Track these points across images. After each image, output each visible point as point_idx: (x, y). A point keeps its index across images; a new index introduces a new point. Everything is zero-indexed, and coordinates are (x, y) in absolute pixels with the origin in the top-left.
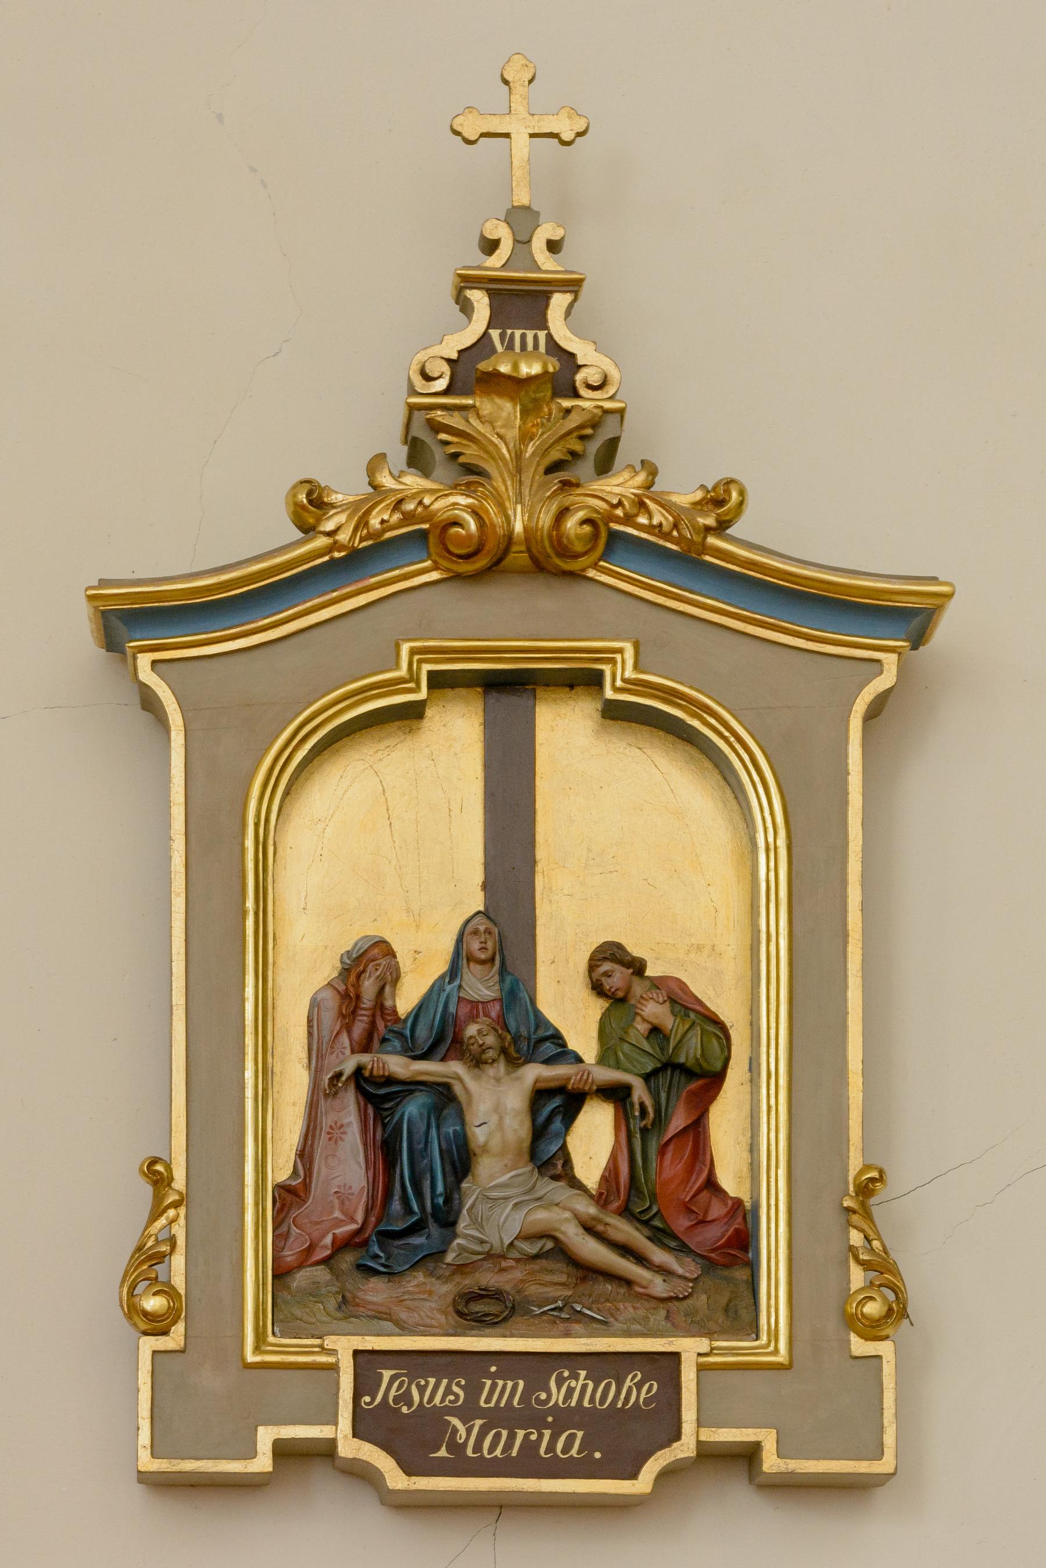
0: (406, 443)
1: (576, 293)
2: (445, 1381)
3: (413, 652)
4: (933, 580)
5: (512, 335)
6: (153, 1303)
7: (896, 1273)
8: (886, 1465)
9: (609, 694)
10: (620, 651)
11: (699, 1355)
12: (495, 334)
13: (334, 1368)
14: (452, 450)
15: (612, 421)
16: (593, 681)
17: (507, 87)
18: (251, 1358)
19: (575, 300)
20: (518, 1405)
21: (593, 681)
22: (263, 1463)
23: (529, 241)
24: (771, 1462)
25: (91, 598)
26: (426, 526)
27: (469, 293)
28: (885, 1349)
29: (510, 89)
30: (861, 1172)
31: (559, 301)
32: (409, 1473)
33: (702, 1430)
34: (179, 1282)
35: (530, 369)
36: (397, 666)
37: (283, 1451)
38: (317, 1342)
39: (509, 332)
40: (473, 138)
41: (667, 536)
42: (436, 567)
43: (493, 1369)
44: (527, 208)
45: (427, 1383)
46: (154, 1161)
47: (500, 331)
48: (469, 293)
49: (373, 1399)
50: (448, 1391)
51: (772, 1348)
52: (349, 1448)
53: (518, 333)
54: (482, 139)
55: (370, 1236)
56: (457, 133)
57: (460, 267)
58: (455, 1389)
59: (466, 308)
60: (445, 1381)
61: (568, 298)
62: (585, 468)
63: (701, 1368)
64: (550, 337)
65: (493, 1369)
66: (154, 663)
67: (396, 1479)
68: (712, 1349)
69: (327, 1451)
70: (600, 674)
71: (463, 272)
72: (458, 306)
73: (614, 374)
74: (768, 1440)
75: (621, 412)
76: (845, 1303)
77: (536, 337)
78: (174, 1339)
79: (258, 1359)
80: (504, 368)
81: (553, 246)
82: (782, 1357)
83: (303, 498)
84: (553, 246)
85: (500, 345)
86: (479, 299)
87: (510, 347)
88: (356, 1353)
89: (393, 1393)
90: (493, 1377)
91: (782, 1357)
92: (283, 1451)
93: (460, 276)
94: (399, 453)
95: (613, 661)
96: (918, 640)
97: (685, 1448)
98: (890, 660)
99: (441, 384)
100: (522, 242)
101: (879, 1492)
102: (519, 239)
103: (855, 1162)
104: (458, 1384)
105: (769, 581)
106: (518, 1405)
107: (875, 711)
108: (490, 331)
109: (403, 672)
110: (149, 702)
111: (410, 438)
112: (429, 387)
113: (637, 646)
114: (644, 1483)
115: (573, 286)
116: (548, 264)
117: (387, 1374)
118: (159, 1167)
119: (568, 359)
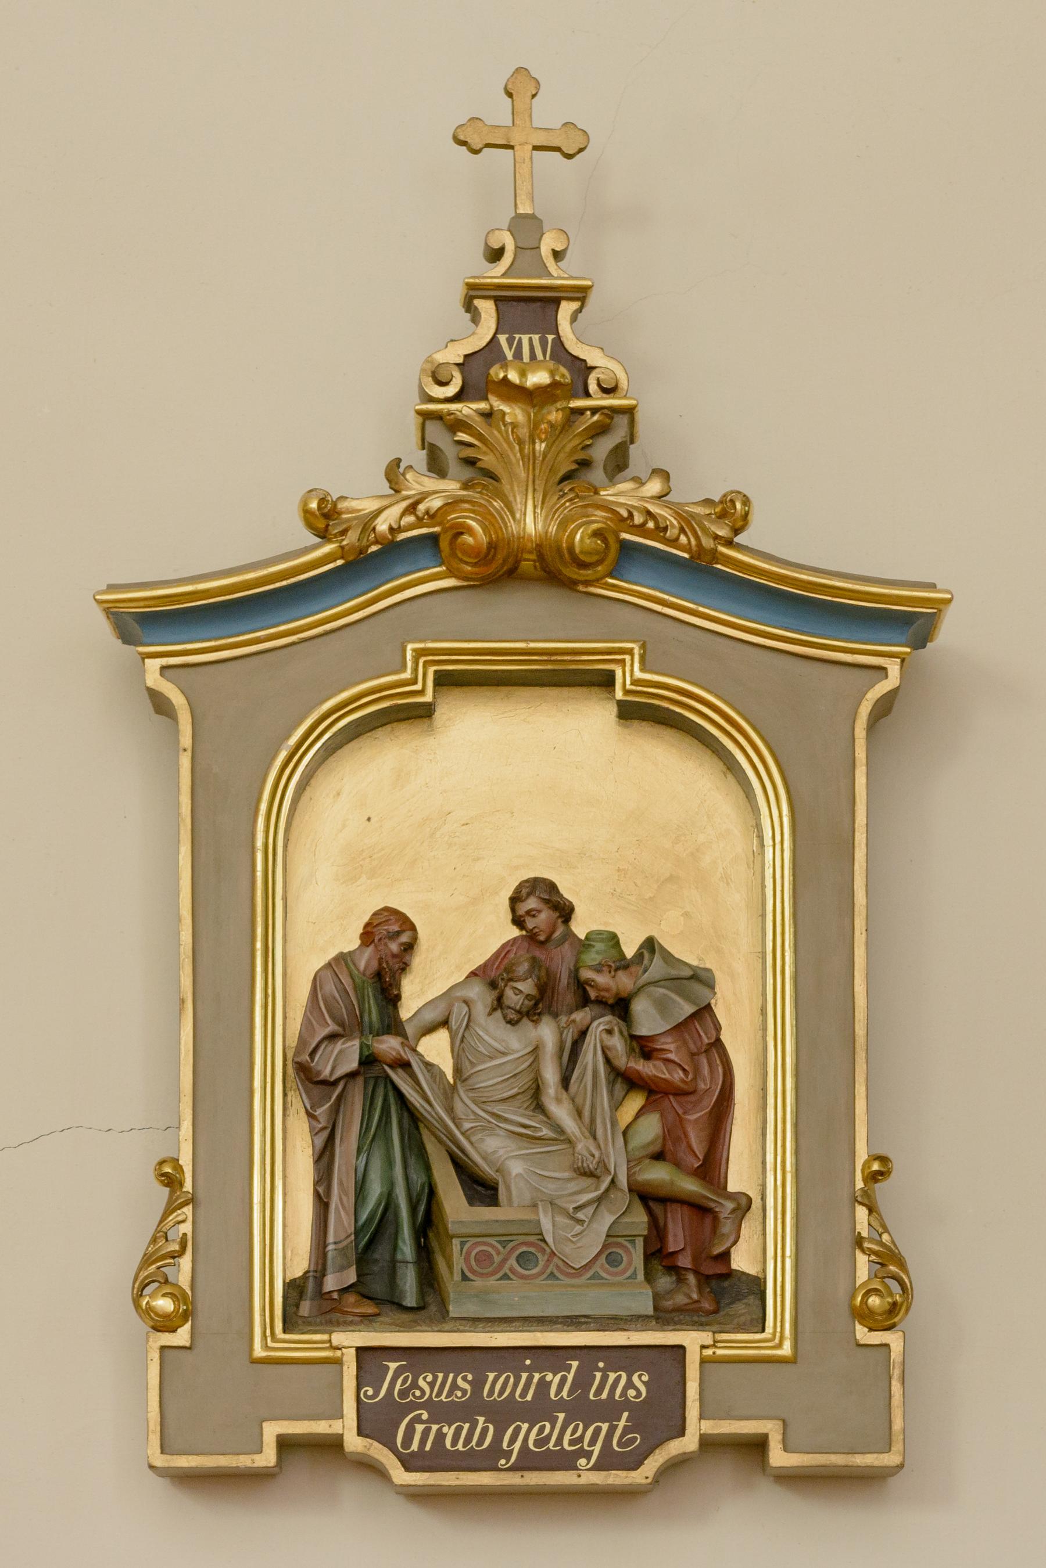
0: (423, 448)
1: (583, 300)
2: (451, 1376)
3: (419, 653)
4: (932, 587)
5: (520, 340)
6: (165, 1304)
7: (902, 1264)
8: (890, 1459)
9: (619, 694)
10: (630, 652)
11: (703, 1347)
12: (502, 339)
13: (338, 1362)
14: (469, 453)
15: (622, 421)
16: (606, 681)
17: (510, 100)
18: (259, 1352)
19: (580, 310)
20: (568, 1397)
21: (606, 681)
22: (268, 1457)
23: (538, 248)
24: (778, 1457)
25: (99, 602)
26: (437, 529)
27: (477, 303)
28: (893, 1339)
29: (513, 101)
30: (866, 1164)
31: (566, 309)
32: (407, 1469)
33: (702, 1421)
34: (184, 1279)
35: (539, 378)
36: (403, 667)
37: (285, 1444)
38: (325, 1337)
39: (517, 336)
40: (477, 147)
41: (674, 542)
42: (451, 573)
43: (528, 1362)
44: (532, 217)
45: (435, 1378)
46: (162, 1163)
47: (507, 336)
48: (477, 303)
49: (376, 1393)
50: (454, 1386)
51: (777, 1341)
52: (354, 1443)
53: (525, 339)
54: (485, 150)
55: (538, 1214)
56: (463, 143)
57: (470, 276)
58: (460, 1382)
59: (476, 318)
60: (451, 1376)
61: (575, 305)
62: (597, 475)
63: (703, 1361)
64: (559, 342)
65: (528, 1362)
66: (163, 668)
67: (400, 1476)
68: (715, 1342)
69: (333, 1445)
70: (611, 675)
71: (471, 280)
72: (468, 315)
73: (624, 383)
74: (771, 1429)
75: (629, 412)
76: (853, 1297)
77: (530, 339)
78: (182, 1336)
79: (264, 1354)
80: (513, 376)
81: (558, 255)
82: (787, 1350)
83: (314, 505)
84: (558, 255)
85: (508, 349)
86: (487, 308)
87: (518, 355)
88: (360, 1350)
89: (398, 1387)
90: (530, 1370)
91: (787, 1350)
92: (285, 1444)
93: (467, 284)
94: (419, 458)
95: (623, 661)
96: (921, 642)
97: (689, 1443)
98: (894, 668)
99: (451, 390)
100: (528, 249)
101: (891, 1481)
102: (520, 245)
103: (862, 1155)
104: (464, 1379)
105: (764, 584)
106: (568, 1397)
107: (885, 707)
108: (499, 336)
109: (407, 675)
110: (160, 705)
111: (426, 444)
112: (622, 389)
113: (643, 646)
114: (640, 1476)
115: (581, 294)
116: (558, 276)
117: (393, 1366)
118: (167, 1169)
119: (582, 369)
